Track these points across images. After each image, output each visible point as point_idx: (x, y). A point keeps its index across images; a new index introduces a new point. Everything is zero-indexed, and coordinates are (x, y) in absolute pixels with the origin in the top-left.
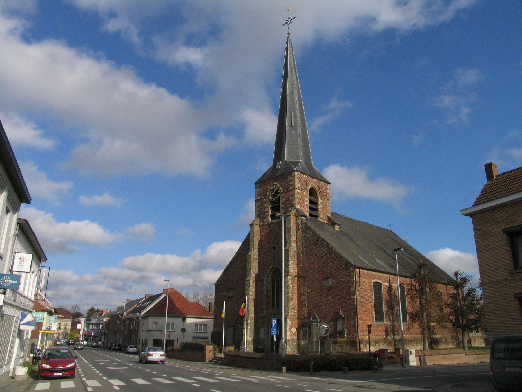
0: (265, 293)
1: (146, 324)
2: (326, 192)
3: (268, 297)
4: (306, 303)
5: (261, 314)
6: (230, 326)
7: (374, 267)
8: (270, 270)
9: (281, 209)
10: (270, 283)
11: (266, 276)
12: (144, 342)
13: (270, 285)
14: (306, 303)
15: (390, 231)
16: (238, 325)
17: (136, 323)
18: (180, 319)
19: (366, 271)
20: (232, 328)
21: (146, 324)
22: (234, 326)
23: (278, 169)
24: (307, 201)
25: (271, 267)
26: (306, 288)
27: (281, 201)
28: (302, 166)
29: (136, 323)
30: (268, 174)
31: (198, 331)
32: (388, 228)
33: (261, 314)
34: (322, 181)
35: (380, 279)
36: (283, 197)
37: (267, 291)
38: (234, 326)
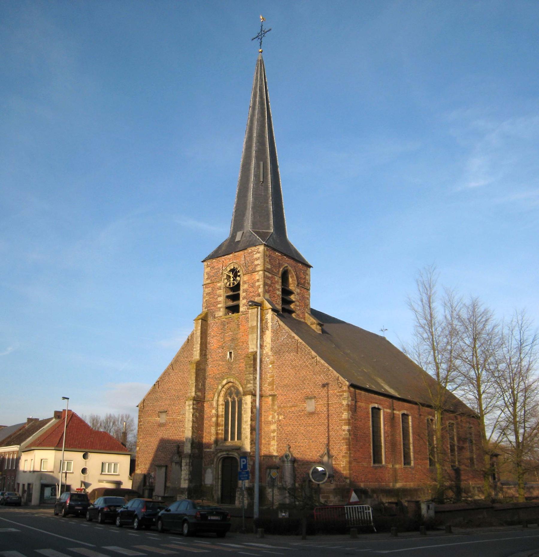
0: (214, 419)
1: (29, 461)
2: (305, 278)
3: (217, 424)
4: (275, 434)
5: (208, 450)
6: (160, 466)
7: (374, 388)
8: (223, 387)
9: (241, 299)
10: (222, 405)
11: (216, 395)
12: (26, 488)
13: (221, 410)
14: (275, 434)
15: (383, 339)
16: (174, 464)
17: (353, 511)
18: (82, 454)
19: (363, 392)
20: (164, 469)
21: (29, 461)
22: (166, 466)
23: (239, 242)
24: (278, 290)
25: (225, 382)
26: (276, 414)
27: (241, 288)
28: (273, 239)
29: (353, 511)
30: (223, 248)
31: (112, 473)
32: (380, 334)
33: (208, 450)
34: (300, 262)
35: (380, 404)
36: (245, 282)
37: (217, 416)
38: (166, 466)
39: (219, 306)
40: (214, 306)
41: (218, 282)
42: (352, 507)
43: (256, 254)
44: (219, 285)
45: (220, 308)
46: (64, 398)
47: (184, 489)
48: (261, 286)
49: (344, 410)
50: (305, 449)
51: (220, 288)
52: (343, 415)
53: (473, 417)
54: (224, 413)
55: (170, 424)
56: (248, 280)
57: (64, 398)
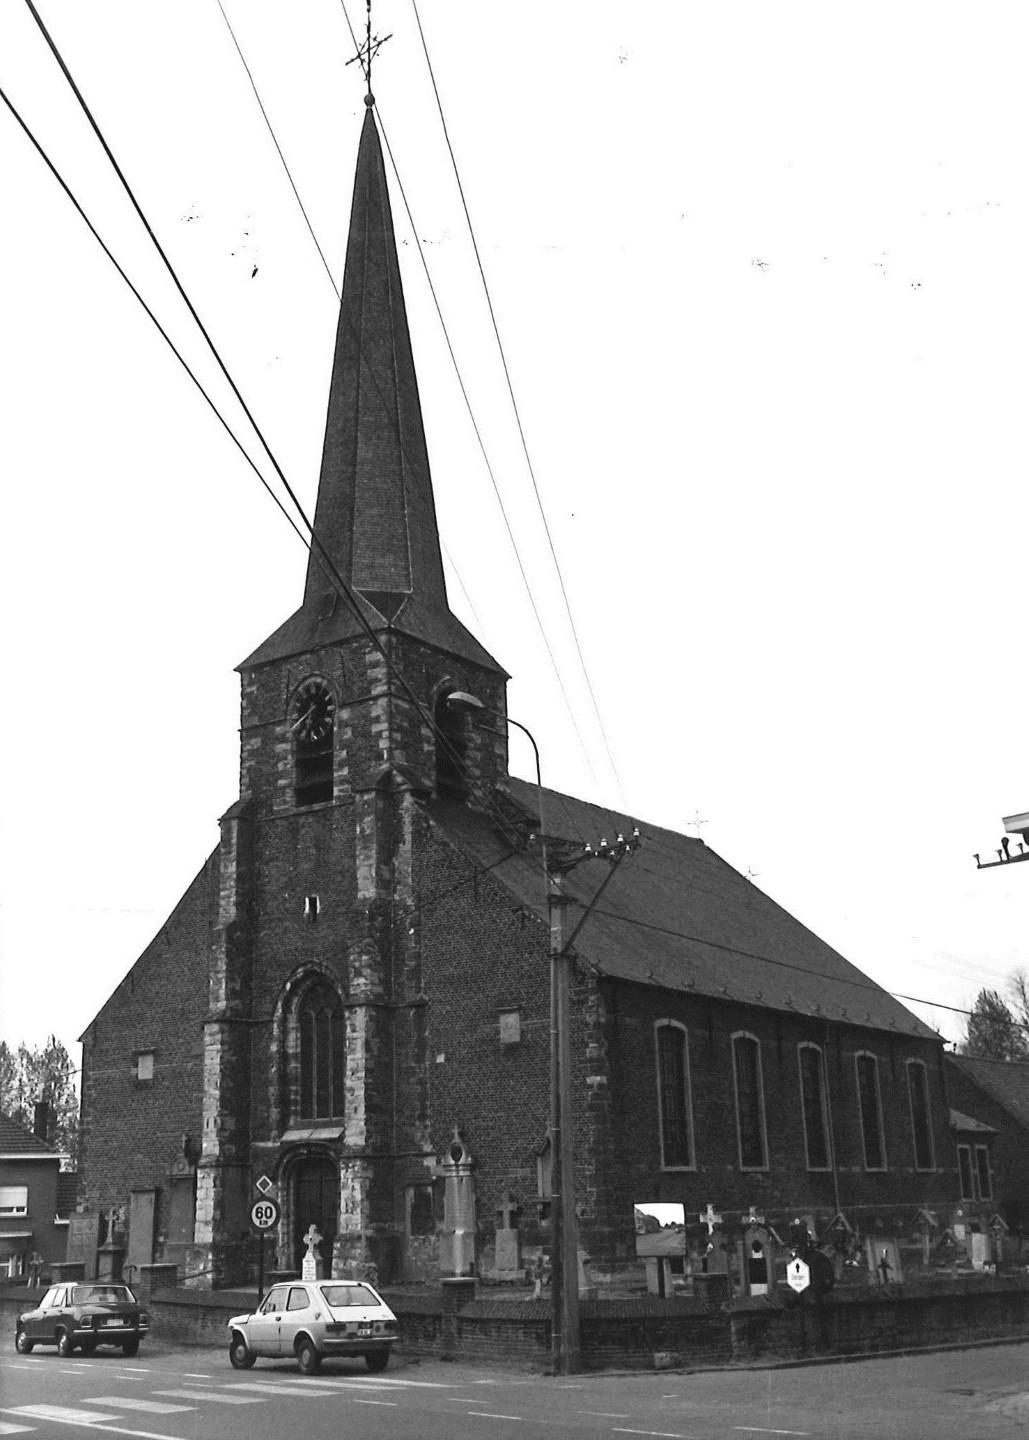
22: (158, 1192)
32: (691, 832)
39: (282, 782)
40: (269, 783)
41: (280, 723)
42: (844, 1155)
43: (370, 652)
44: (279, 730)
45: (284, 788)
46: (255, 271)
47: (204, 1246)
48: (385, 734)
49: (590, 1036)
50: (499, 1135)
51: (283, 739)
52: (588, 1050)
53: (495, 1285)
54: (299, 1050)
55: (166, 1083)
56: (350, 718)
57: (255, 271)
